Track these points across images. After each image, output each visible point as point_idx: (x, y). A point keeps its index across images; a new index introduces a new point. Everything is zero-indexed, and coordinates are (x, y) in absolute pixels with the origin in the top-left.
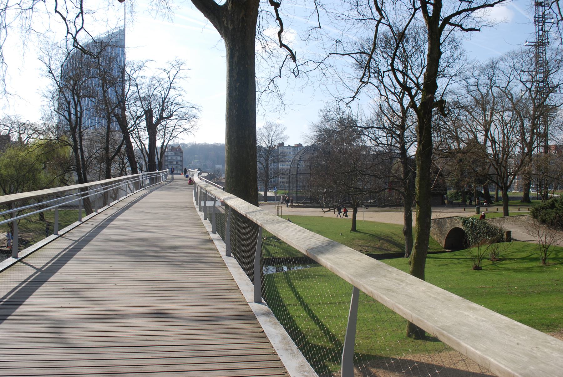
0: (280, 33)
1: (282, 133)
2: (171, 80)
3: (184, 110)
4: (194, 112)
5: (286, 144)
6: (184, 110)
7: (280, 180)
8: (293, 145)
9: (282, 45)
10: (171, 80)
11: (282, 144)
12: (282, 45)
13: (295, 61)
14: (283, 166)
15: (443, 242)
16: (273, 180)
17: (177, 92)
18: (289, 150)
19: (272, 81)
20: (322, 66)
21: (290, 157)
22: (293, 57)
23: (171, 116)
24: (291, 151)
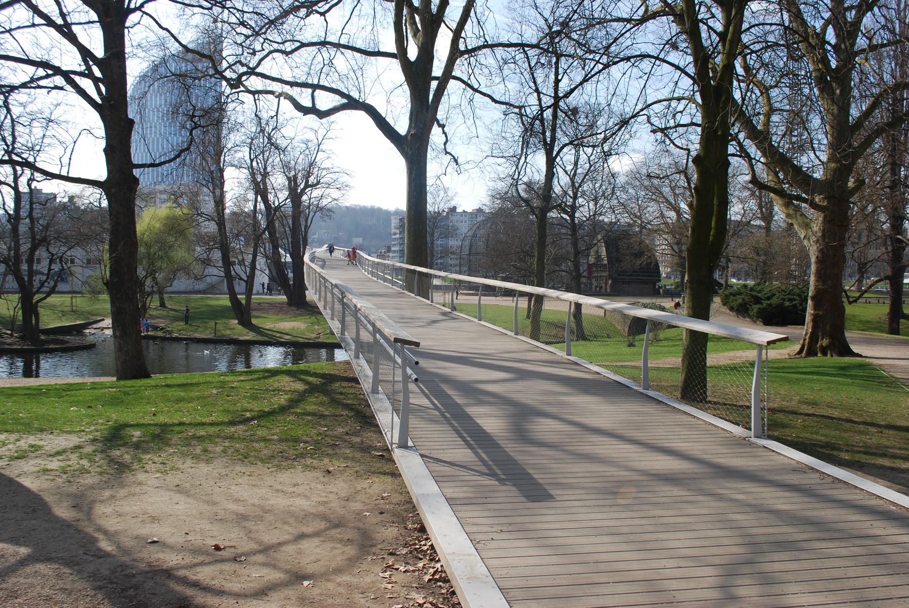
0: (445, 144)
1: (452, 199)
2: (320, 140)
3: (334, 176)
4: (344, 178)
5: (459, 210)
6: (334, 176)
7: (450, 262)
8: (470, 210)
9: (447, 153)
10: (320, 140)
11: (455, 208)
12: (447, 153)
13: (457, 164)
14: (454, 243)
15: (626, 330)
16: (439, 261)
17: (326, 155)
18: (464, 218)
19: (439, 177)
20: (481, 165)
21: (464, 228)
22: (456, 161)
23: (318, 183)
24: (466, 219)
